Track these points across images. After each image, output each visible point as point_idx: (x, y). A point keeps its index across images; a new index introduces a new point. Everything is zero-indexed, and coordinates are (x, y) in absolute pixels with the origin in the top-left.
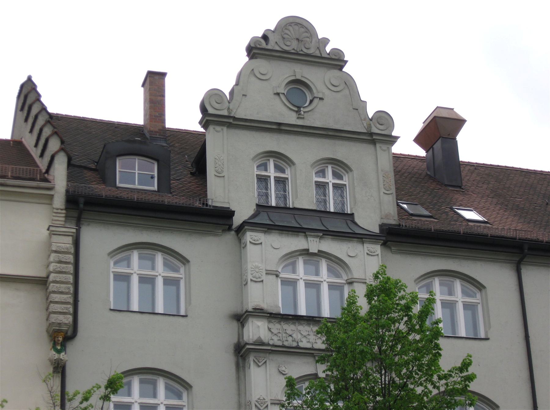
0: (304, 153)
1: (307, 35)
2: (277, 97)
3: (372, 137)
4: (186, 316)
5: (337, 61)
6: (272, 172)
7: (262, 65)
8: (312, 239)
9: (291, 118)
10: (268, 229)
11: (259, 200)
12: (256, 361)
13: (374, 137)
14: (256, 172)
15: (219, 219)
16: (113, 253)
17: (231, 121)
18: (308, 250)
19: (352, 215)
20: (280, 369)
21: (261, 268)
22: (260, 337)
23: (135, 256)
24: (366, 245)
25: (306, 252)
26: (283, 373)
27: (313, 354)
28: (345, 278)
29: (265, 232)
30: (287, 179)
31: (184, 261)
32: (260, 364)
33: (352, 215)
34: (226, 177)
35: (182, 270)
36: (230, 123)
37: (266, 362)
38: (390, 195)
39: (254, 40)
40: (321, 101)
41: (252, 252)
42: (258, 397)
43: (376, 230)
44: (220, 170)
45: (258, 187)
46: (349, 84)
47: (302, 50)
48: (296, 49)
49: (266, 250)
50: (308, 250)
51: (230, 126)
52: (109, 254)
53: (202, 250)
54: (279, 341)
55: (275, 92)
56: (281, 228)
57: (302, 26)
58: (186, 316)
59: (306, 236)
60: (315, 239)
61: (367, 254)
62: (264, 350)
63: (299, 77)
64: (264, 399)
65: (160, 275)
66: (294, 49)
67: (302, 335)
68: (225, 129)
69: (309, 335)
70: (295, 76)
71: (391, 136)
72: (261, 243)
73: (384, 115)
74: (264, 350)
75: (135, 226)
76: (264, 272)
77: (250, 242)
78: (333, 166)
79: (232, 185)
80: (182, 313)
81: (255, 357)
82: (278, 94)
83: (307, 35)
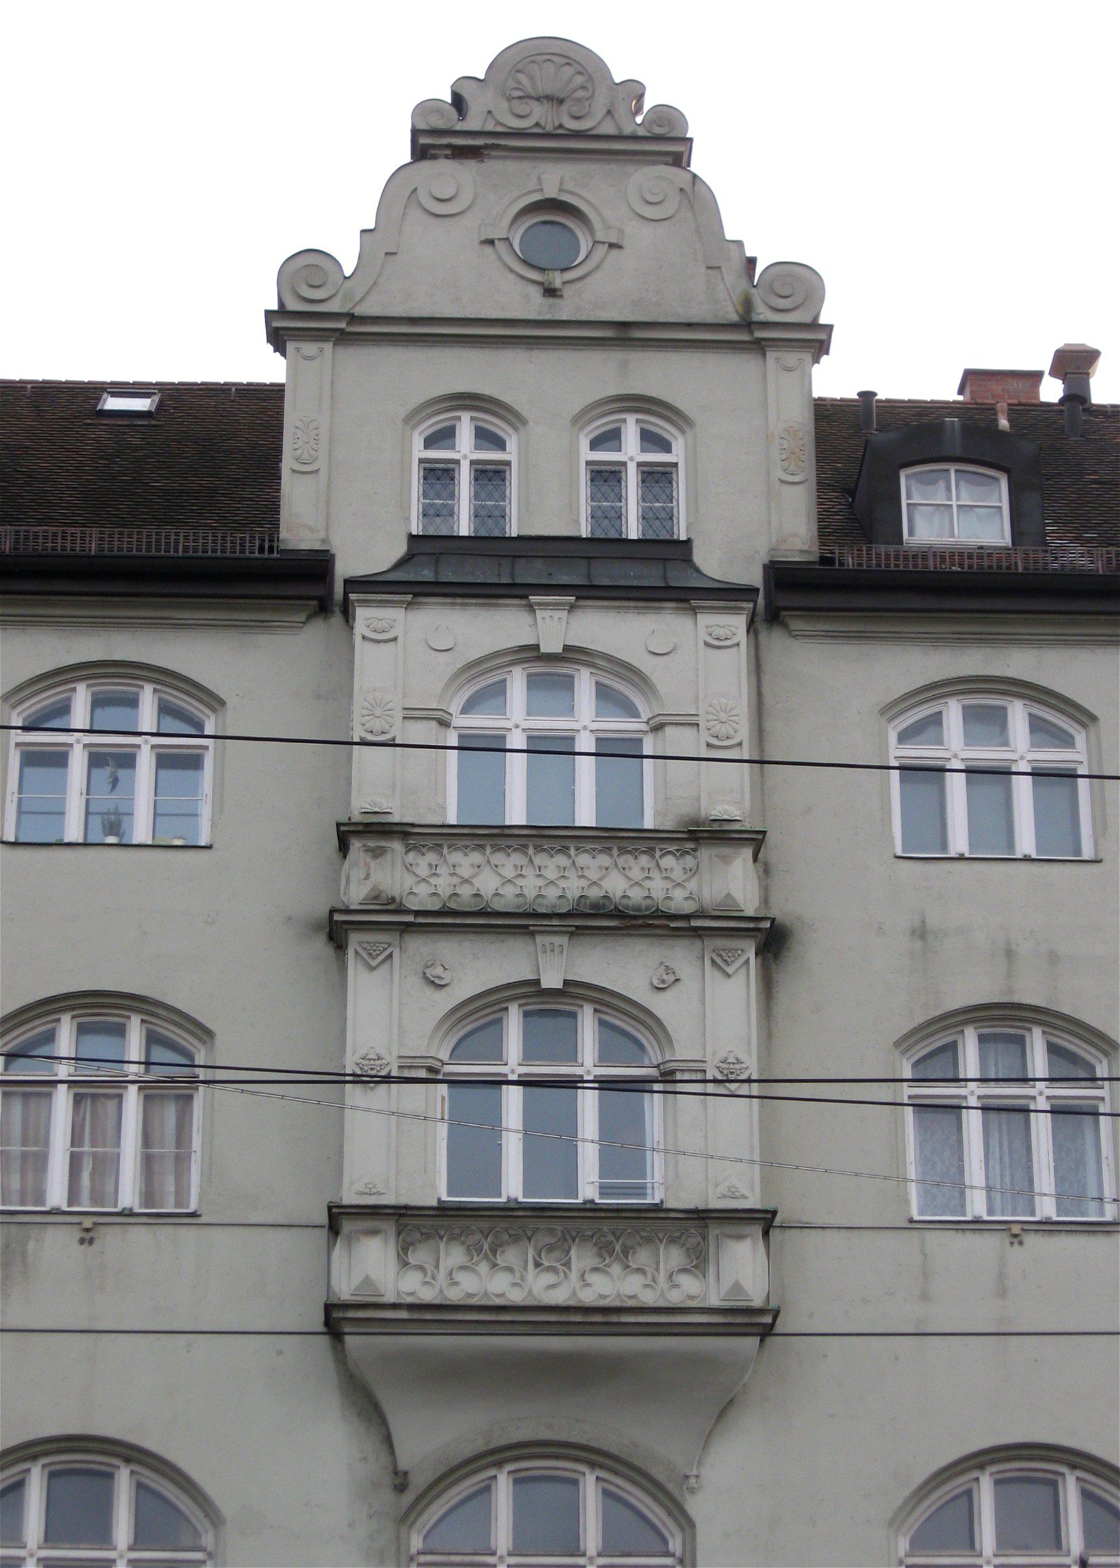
0: (551, 390)
1: (579, 80)
2: (488, 250)
3: (751, 332)
4: (209, 847)
5: (665, 143)
6: (631, 451)
7: (448, 175)
8: (547, 614)
9: (533, 306)
10: (416, 595)
11: (424, 527)
12: (718, 961)
13: (759, 334)
14: (587, 454)
15: (305, 586)
16: (892, 709)
17: (342, 325)
18: (536, 647)
19: (688, 542)
20: (428, 971)
21: (390, 705)
22: (729, 896)
23: (953, 712)
24: (704, 619)
25: (530, 653)
26: (437, 981)
27: (527, 926)
28: (645, 713)
29: (409, 605)
30: (675, 465)
31: (1084, 719)
32: (730, 970)
33: (688, 542)
34: (323, 473)
35: (1080, 739)
36: (342, 331)
37: (391, 955)
38: (802, 486)
39: (424, 109)
40: (615, 253)
41: (371, 664)
42: (722, 1054)
43: (754, 577)
44: (306, 456)
45: (424, 492)
46: (697, 200)
47: (561, 126)
48: (542, 123)
49: (408, 654)
50: (536, 647)
51: (342, 338)
52: (883, 711)
53: (244, 666)
54: (690, 902)
55: (483, 238)
56: (645, 595)
57: (569, 62)
58: (209, 847)
59: (531, 608)
60: (557, 614)
61: (707, 644)
62: (397, 921)
63: (551, 192)
64: (739, 1061)
65: (955, 756)
66: (537, 125)
67: (630, 879)
68: (328, 347)
69: (648, 878)
70: (541, 190)
71: (814, 325)
72: (395, 639)
73: (778, 268)
74: (397, 921)
75: (961, 640)
76: (399, 715)
77: (364, 638)
78: (475, 414)
79: (348, 495)
80: (1087, 853)
81: (361, 943)
82: (491, 242)
83: (579, 80)
